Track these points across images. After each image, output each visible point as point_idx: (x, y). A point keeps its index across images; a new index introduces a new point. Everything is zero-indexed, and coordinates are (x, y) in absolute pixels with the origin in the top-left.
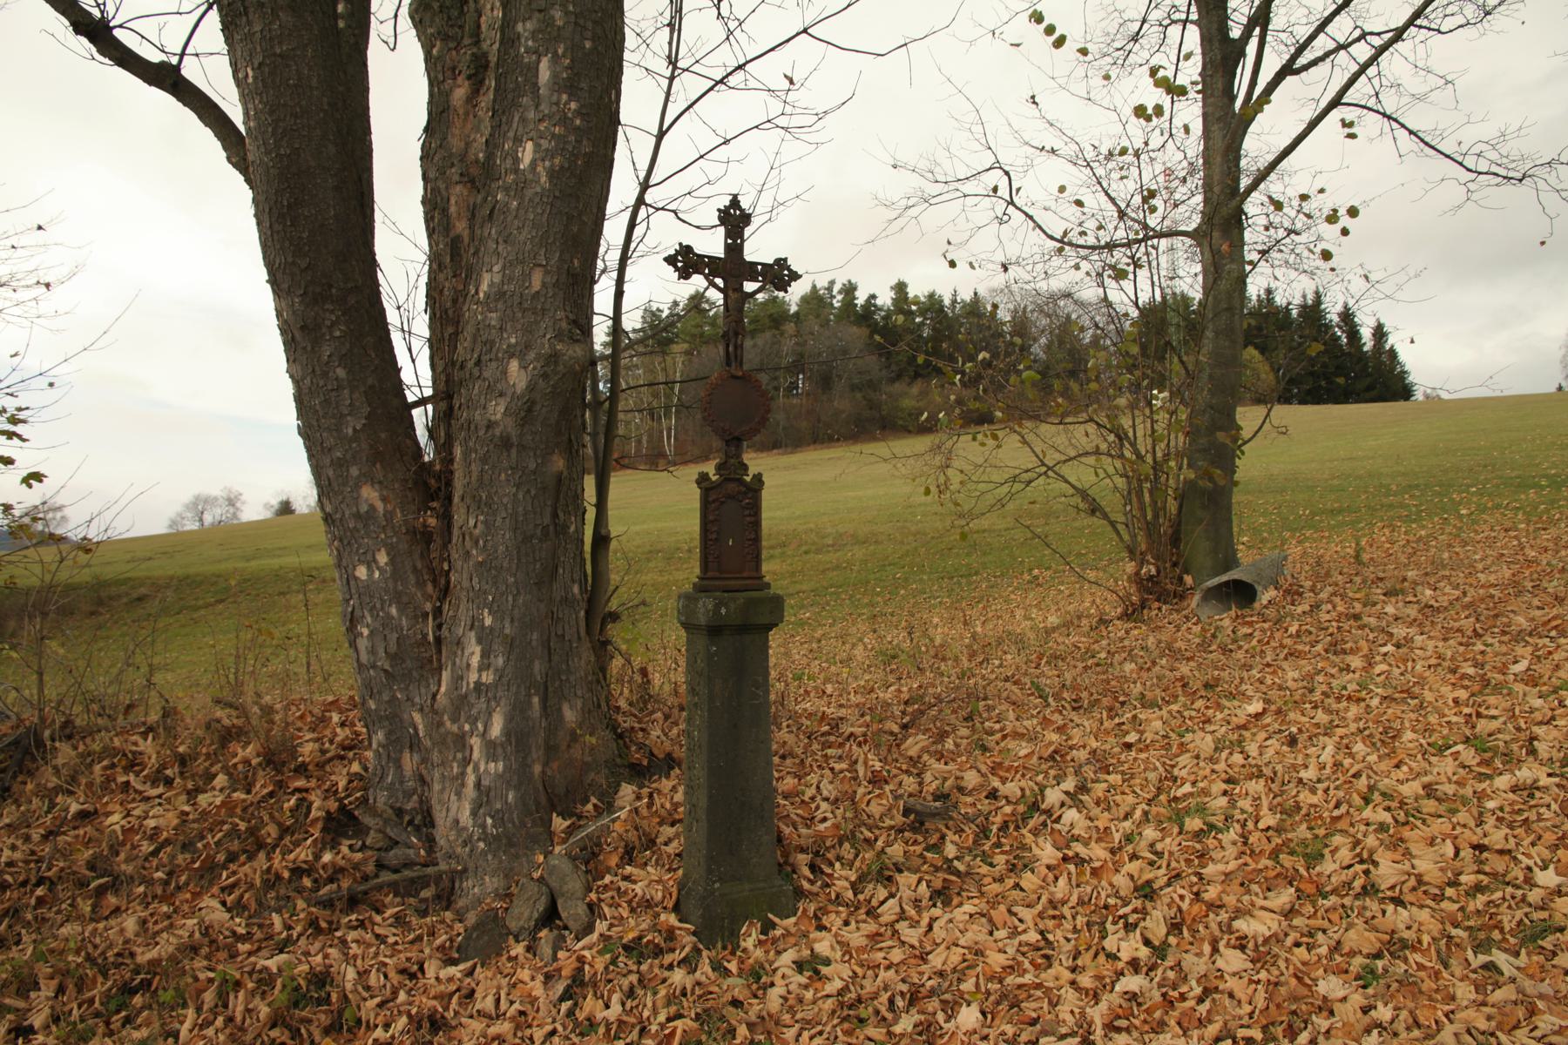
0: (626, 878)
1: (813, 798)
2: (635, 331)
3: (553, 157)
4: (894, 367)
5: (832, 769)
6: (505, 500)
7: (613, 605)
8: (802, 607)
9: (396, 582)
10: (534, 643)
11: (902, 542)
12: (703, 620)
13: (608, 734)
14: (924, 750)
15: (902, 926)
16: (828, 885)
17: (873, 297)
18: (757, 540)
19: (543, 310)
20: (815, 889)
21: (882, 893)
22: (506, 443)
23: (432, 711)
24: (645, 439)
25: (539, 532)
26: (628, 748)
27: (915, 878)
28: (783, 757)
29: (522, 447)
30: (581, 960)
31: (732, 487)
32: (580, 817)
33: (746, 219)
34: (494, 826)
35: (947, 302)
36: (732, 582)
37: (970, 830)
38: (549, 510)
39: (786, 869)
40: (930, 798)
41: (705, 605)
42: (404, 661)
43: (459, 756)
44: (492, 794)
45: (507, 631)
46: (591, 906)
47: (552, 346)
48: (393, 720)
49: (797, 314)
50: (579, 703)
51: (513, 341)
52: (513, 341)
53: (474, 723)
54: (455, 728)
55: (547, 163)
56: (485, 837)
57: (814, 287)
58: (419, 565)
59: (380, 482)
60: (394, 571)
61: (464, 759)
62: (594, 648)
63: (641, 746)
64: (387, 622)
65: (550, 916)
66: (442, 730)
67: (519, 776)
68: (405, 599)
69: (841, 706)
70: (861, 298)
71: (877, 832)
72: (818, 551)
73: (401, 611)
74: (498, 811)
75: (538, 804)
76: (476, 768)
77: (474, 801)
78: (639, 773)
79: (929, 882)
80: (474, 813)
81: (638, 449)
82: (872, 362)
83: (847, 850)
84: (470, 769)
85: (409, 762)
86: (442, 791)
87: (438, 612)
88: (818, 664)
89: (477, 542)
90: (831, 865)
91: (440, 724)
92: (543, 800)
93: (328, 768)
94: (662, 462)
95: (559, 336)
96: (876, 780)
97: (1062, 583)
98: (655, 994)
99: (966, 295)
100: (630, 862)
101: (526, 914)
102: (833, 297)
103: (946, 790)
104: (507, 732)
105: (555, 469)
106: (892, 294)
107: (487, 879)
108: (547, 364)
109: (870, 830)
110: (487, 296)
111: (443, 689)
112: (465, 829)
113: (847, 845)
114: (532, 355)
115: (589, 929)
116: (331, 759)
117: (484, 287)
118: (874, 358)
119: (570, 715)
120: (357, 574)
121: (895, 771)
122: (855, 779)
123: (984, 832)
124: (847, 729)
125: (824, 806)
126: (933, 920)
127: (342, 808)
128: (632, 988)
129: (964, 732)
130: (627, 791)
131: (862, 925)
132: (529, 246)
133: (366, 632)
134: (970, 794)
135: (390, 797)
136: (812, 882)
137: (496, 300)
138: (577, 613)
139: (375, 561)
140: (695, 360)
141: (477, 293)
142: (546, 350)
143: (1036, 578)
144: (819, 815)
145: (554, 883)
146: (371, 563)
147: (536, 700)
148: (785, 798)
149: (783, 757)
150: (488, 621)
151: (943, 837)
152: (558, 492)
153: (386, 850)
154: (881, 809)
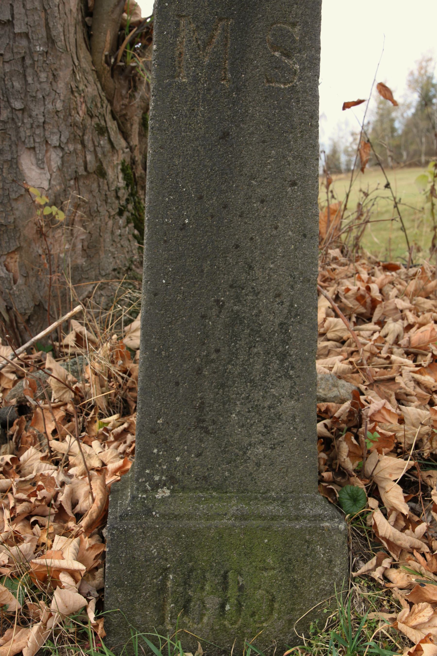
20: (406, 539)
50: (55, 158)
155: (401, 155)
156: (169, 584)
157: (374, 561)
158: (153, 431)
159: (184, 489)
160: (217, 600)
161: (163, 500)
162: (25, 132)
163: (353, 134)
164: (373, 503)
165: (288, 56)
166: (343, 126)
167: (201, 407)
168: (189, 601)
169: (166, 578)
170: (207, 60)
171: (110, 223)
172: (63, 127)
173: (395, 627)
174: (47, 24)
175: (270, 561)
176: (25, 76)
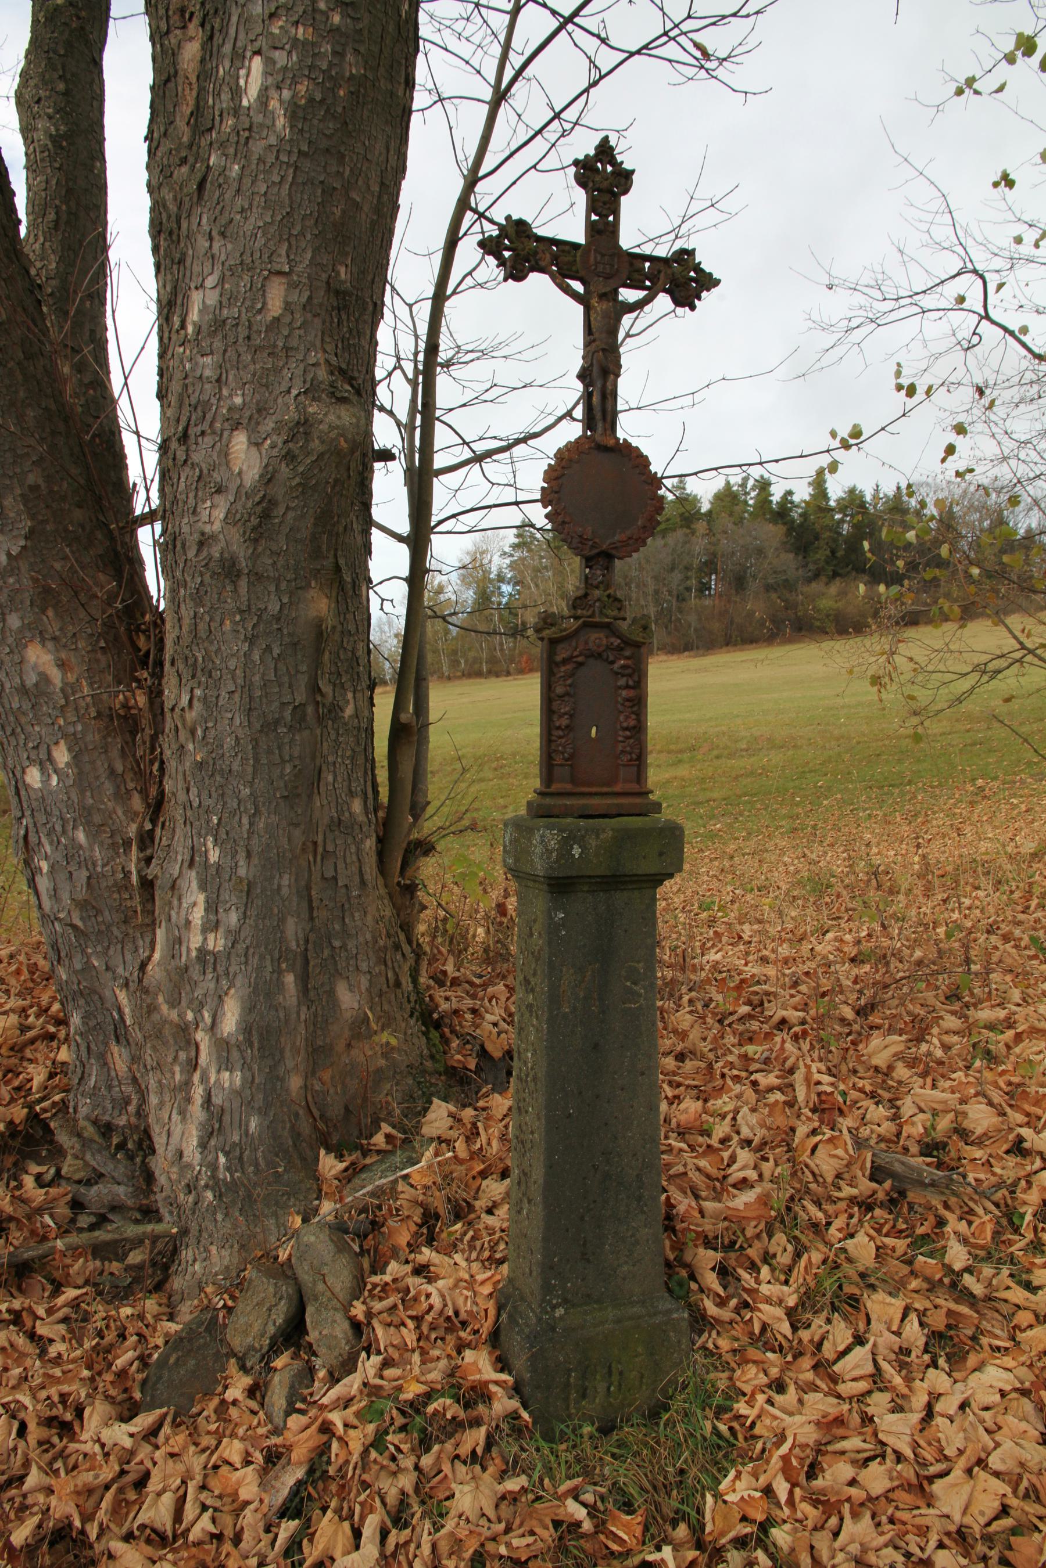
0: (421, 1270)
1: (723, 1141)
3: (294, 82)
4: (811, 566)
5: (755, 1083)
6: (232, 664)
7: (428, 826)
8: (712, 817)
9: (82, 792)
10: (285, 891)
11: (824, 747)
12: (539, 867)
13: (415, 1026)
14: (898, 1056)
15: (879, 1402)
16: (746, 1305)
17: (790, 493)
18: (639, 729)
19: (287, 349)
20: (726, 1314)
21: (841, 1334)
22: (229, 570)
23: (140, 987)
25: (287, 714)
26: (446, 1042)
27: (898, 1304)
28: (681, 1057)
29: (257, 577)
30: (326, 1428)
31: (596, 639)
32: (365, 1153)
33: (624, 179)
34: (228, 1169)
35: (868, 498)
36: (595, 801)
37: (986, 1219)
38: (303, 680)
39: (677, 1275)
40: (914, 1149)
41: (546, 839)
42: (99, 912)
43: (183, 1056)
44: (227, 1118)
45: (242, 872)
46: (357, 1327)
47: (300, 408)
48: (87, 993)
49: (710, 513)
50: (364, 981)
51: (238, 400)
52: (238, 400)
53: (198, 1011)
54: (174, 1015)
55: (286, 94)
56: (215, 1184)
57: (728, 483)
58: (119, 768)
59: (54, 639)
60: (80, 774)
61: (189, 1061)
62: (391, 896)
63: (467, 1040)
64: (72, 854)
65: (293, 1333)
66: (156, 1017)
67: (266, 1091)
68: (97, 819)
69: (764, 960)
70: (777, 494)
71: (830, 1208)
72: (731, 756)
73: (93, 834)
74: (234, 1145)
75: (296, 1135)
76: (205, 1079)
77: (202, 1126)
78: (461, 1085)
79: (922, 1314)
80: (203, 1145)
82: (788, 560)
83: (780, 1244)
84: (196, 1077)
85: (119, 1058)
86: (161, 1104)
87: (146, 840)
88: (730, 908)
89: (193, 732)
90: (754, 1268)
91: (152, 1009)
92: (305, 1126)
93: (28, 1053)
95: (311, 391)
96: (826, 1110)
97: (1014, 796)
98: (437, 1528)
99: (888, 489)
100: (430, 1241)
101: (257, 1326)
102: (747, 494)
103: (939, 1135)
104: (246, 1028)
105: (312, 613)
106: (810, 490)
107: (214, 1249)
108: (292, 438)
109: (818, 1204)
110: (198, 331)
111: (157, 956)
112: (189, 1166)
113: (780, 1238)
114: (269, 424)
115: (349, 1366)
116: (32, 1041)
117: (194, 316)
118: (791, 556)
119: (349, 999)
120: (28, 779)
121: (854, 1094)
122: (791, 1104)
123: (1010, 1218)
124: (776, 1011)
125: (744, 1156)
126: (935, 1397)
127: (33, 1117)
128: (403, 1502)
129: (951, 1022)
130: (439, 1116)
131: (810, 1398)
132: (260, 241)
133: (45, 866)
134: (979, 1143)
135: (95, 1107)
136: (722, 1303)
137: (213, 334)
138: (358, 845)
139: (50, 758)
141: (183, 326)
142: (291, 415)
143: (981, 789)
144: (736, 1173)
145: (305, 1275)
146: (46, 763)
147: (290, 979)
148: (681, 1135)
149: (681, 1057)
150: (214, 856)
151: (941, 1223)
152: (319, 652)
153: (89, 1183)
154: (836, 1164)
155: (459, 662)
156: (572, 1380)
157: (706, 1334)
158: (551, 1268)
159: (573, 1306)
160: (605, 1385)
161: (561, 1318)
162: (342, 964)
163: (396, 636)
164: (694, 1286)
165: (635, 984)
166: (386, 628)
167: (584, 1244)
168: (586, 1389)
169: (569, 1376)
170: (582, 994)
171: (403, 1025)
172: (371, 954)
173: (734, 1385)
174: (361, 871)
175: (640, 1350)
176: (343, 918)
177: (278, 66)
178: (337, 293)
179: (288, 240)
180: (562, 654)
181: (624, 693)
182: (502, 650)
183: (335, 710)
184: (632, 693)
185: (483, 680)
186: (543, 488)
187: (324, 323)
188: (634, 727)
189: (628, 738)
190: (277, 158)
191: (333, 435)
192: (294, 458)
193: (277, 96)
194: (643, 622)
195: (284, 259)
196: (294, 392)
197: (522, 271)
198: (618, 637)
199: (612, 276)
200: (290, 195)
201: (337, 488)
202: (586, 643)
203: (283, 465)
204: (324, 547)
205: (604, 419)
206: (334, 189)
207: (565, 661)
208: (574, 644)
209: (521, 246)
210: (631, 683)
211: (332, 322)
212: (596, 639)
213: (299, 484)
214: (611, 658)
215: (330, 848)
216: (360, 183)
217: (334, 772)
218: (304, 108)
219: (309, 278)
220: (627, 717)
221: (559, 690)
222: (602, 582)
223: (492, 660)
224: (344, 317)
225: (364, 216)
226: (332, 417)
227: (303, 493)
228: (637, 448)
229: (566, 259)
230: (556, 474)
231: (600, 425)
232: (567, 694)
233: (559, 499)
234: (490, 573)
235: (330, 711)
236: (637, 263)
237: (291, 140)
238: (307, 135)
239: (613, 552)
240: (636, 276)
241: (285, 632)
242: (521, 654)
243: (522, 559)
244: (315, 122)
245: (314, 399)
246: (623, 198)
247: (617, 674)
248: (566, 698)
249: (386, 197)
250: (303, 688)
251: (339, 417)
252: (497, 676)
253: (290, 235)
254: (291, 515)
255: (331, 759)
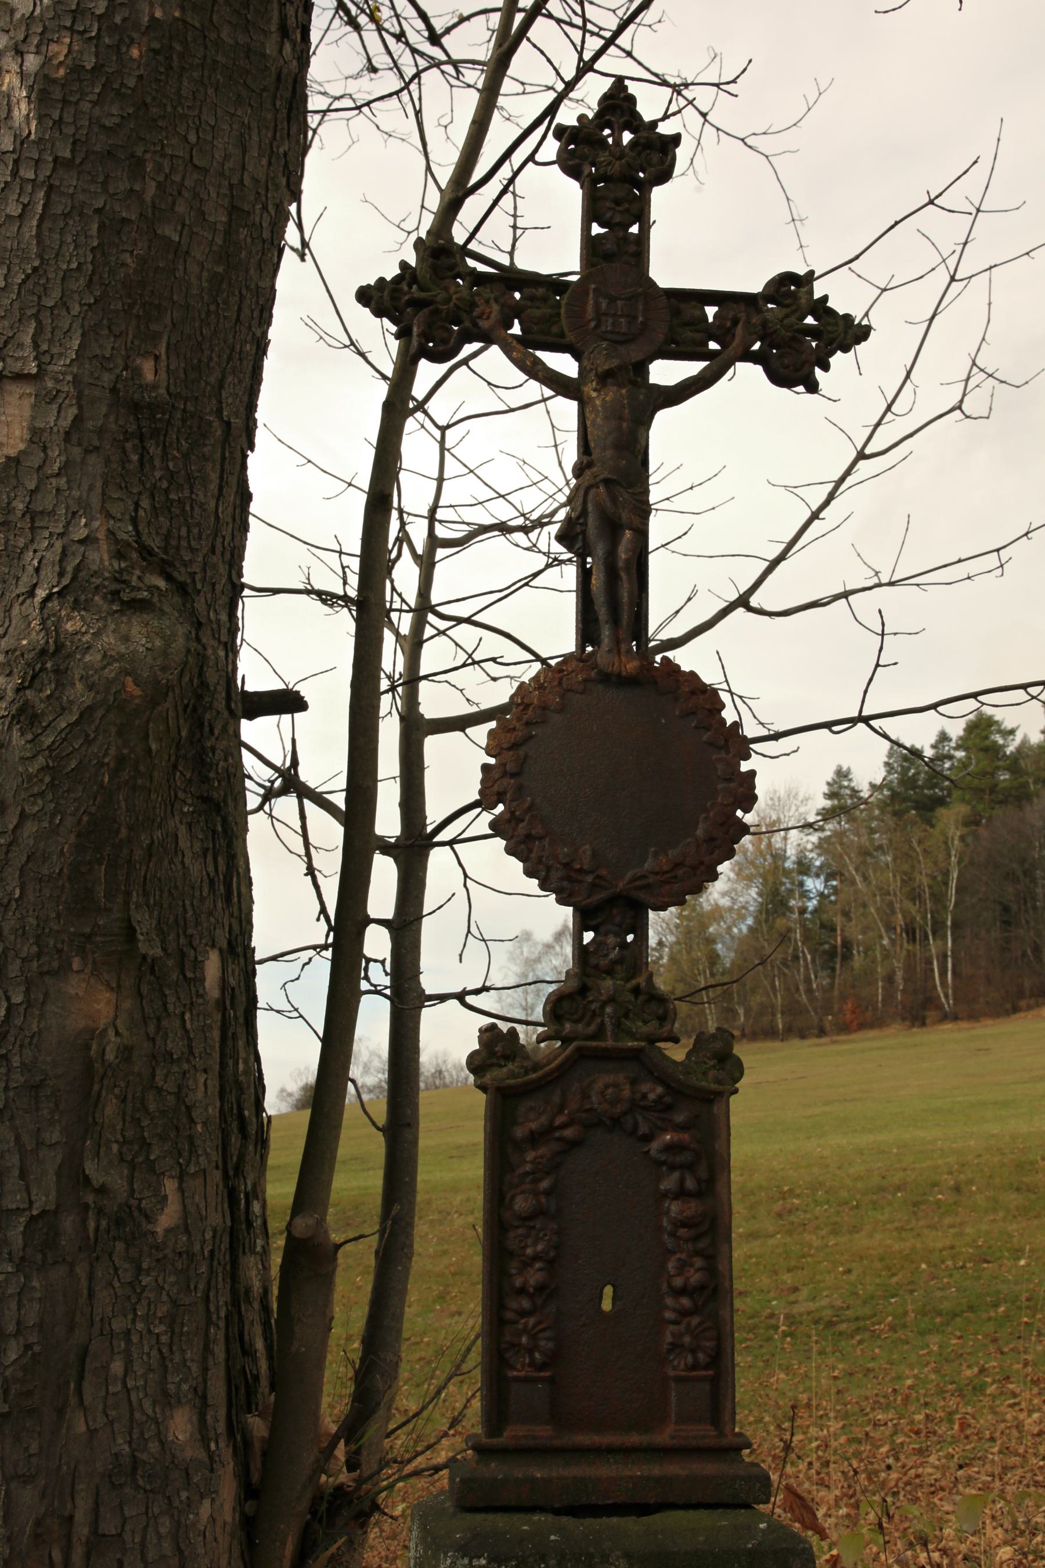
2: (873, 787)
3: (45, 39)
18: (712, 1292)
24: (899, 975)
33: (657, 155)
36: (605, 1470)
55: (32, 62)
81: (889, 997)
94: (931, 1014)
95: (73, 591)
108: (32, 681)
140: (983, 832)
142: (32, 638)
155: (735, 1013)
177: (18, 16)
178: (135, 407)
179: (36, 316)
180: (530, 1120)
181: (675, 1208)
182: (809, 991)
183: (129, 1221)
184: (692, 1208)
185: (777, 1044)
186: (485, 767)
187: (108, 462)
188: (702, 1288)
189: (684, 1313)
190: (15, 173)
191: (110, 672)
192: (34, 718)
193: (15, 67)
194: (718, 1045)
195: (28, 352)
196: (41, 593)
197: (445, 341)
198: (661, 1081)
199: (620, 336)
200: (39, 236)
201: (125, 776)
202: (585, 1095)
203: (16, 734)
204: (100, 891)
205: (615, 620)
206: (125, 221)
207: (534, 1139)
208: (556, 1099)
209: (442, 296)
210: (690, 1184)
211: (125, 460)
212: (606, 1085)
213: (45, 768)
214: (643, 1129)
215: (109, 1526)
216: (181, 208)
217: (127, 1354)
218: (64, 84)
219: (76, 381)
220: (682, 1266)
221: (521, 1204)
222: (619, 961)
223: (793, 1009)
224: (154, 449)
225: (194, 268)
226: (109, 639)
227: (52, 785)
228: (693, 675)
229: (537, 313)
230: (512, 737)
231: (606, 632)
232: (538, 1213)
233: (520, 789)
234: (785, 858)
235: (118, 1222)
236: (689, 310)
237: (40, 140)
238: (70, 130)
239: (642, 896)
240: (688, 334)
241: (16, 1061)
242: (843, 998)
243: (839, 835)
244: (85, 106)
245: (76, 606)
246: (658, 194)
247: (660, 1163)
248: (538, 1223)
249: (243, 233)
250: (51, 1178)
251: (126, 639)
252: (803, 1037)
253: (41, 307)
254: (30, 828)
255: (118, 1325)
